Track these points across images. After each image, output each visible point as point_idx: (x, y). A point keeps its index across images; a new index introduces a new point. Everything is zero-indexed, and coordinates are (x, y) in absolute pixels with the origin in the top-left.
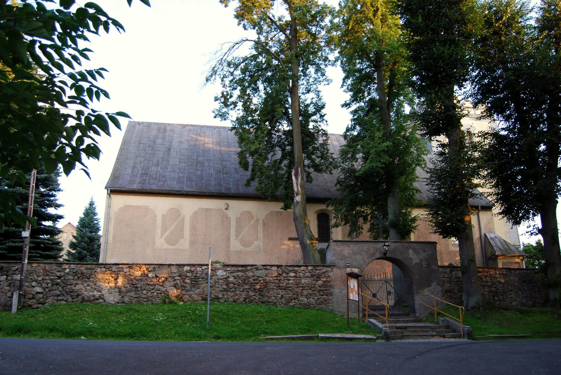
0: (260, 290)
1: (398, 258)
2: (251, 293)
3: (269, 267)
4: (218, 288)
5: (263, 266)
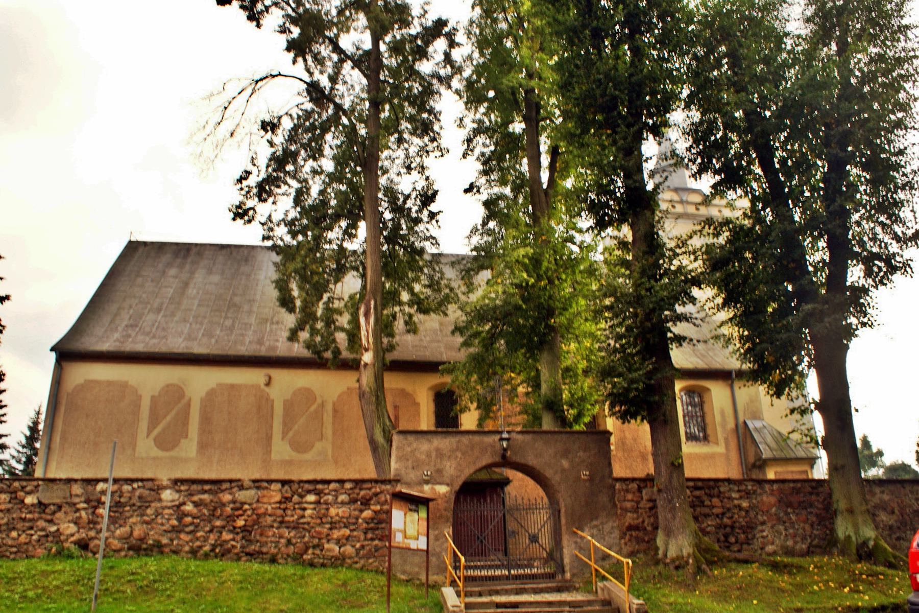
0: (244, 529)
1: (530, 463)
2: (226, 536)
3: (265, 484)
4: (162, 524)
5: (255, 481)
